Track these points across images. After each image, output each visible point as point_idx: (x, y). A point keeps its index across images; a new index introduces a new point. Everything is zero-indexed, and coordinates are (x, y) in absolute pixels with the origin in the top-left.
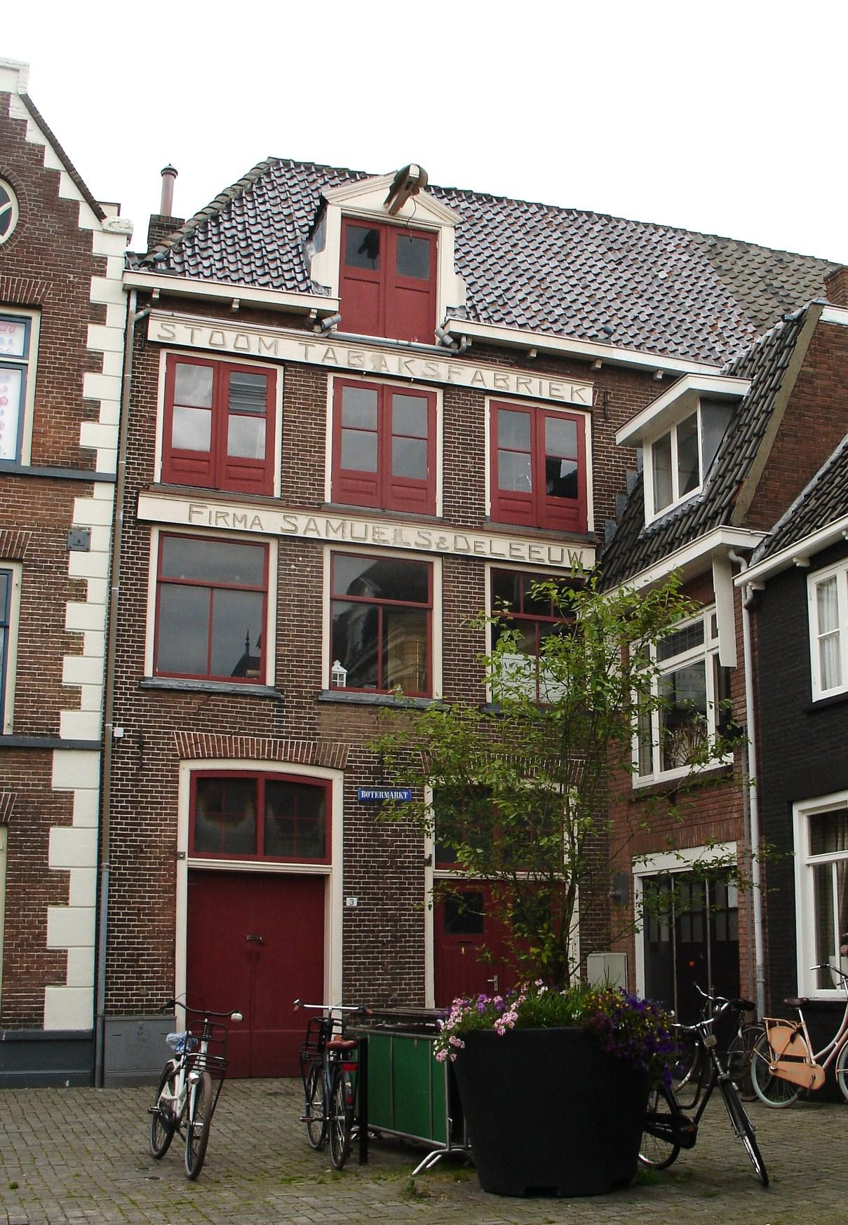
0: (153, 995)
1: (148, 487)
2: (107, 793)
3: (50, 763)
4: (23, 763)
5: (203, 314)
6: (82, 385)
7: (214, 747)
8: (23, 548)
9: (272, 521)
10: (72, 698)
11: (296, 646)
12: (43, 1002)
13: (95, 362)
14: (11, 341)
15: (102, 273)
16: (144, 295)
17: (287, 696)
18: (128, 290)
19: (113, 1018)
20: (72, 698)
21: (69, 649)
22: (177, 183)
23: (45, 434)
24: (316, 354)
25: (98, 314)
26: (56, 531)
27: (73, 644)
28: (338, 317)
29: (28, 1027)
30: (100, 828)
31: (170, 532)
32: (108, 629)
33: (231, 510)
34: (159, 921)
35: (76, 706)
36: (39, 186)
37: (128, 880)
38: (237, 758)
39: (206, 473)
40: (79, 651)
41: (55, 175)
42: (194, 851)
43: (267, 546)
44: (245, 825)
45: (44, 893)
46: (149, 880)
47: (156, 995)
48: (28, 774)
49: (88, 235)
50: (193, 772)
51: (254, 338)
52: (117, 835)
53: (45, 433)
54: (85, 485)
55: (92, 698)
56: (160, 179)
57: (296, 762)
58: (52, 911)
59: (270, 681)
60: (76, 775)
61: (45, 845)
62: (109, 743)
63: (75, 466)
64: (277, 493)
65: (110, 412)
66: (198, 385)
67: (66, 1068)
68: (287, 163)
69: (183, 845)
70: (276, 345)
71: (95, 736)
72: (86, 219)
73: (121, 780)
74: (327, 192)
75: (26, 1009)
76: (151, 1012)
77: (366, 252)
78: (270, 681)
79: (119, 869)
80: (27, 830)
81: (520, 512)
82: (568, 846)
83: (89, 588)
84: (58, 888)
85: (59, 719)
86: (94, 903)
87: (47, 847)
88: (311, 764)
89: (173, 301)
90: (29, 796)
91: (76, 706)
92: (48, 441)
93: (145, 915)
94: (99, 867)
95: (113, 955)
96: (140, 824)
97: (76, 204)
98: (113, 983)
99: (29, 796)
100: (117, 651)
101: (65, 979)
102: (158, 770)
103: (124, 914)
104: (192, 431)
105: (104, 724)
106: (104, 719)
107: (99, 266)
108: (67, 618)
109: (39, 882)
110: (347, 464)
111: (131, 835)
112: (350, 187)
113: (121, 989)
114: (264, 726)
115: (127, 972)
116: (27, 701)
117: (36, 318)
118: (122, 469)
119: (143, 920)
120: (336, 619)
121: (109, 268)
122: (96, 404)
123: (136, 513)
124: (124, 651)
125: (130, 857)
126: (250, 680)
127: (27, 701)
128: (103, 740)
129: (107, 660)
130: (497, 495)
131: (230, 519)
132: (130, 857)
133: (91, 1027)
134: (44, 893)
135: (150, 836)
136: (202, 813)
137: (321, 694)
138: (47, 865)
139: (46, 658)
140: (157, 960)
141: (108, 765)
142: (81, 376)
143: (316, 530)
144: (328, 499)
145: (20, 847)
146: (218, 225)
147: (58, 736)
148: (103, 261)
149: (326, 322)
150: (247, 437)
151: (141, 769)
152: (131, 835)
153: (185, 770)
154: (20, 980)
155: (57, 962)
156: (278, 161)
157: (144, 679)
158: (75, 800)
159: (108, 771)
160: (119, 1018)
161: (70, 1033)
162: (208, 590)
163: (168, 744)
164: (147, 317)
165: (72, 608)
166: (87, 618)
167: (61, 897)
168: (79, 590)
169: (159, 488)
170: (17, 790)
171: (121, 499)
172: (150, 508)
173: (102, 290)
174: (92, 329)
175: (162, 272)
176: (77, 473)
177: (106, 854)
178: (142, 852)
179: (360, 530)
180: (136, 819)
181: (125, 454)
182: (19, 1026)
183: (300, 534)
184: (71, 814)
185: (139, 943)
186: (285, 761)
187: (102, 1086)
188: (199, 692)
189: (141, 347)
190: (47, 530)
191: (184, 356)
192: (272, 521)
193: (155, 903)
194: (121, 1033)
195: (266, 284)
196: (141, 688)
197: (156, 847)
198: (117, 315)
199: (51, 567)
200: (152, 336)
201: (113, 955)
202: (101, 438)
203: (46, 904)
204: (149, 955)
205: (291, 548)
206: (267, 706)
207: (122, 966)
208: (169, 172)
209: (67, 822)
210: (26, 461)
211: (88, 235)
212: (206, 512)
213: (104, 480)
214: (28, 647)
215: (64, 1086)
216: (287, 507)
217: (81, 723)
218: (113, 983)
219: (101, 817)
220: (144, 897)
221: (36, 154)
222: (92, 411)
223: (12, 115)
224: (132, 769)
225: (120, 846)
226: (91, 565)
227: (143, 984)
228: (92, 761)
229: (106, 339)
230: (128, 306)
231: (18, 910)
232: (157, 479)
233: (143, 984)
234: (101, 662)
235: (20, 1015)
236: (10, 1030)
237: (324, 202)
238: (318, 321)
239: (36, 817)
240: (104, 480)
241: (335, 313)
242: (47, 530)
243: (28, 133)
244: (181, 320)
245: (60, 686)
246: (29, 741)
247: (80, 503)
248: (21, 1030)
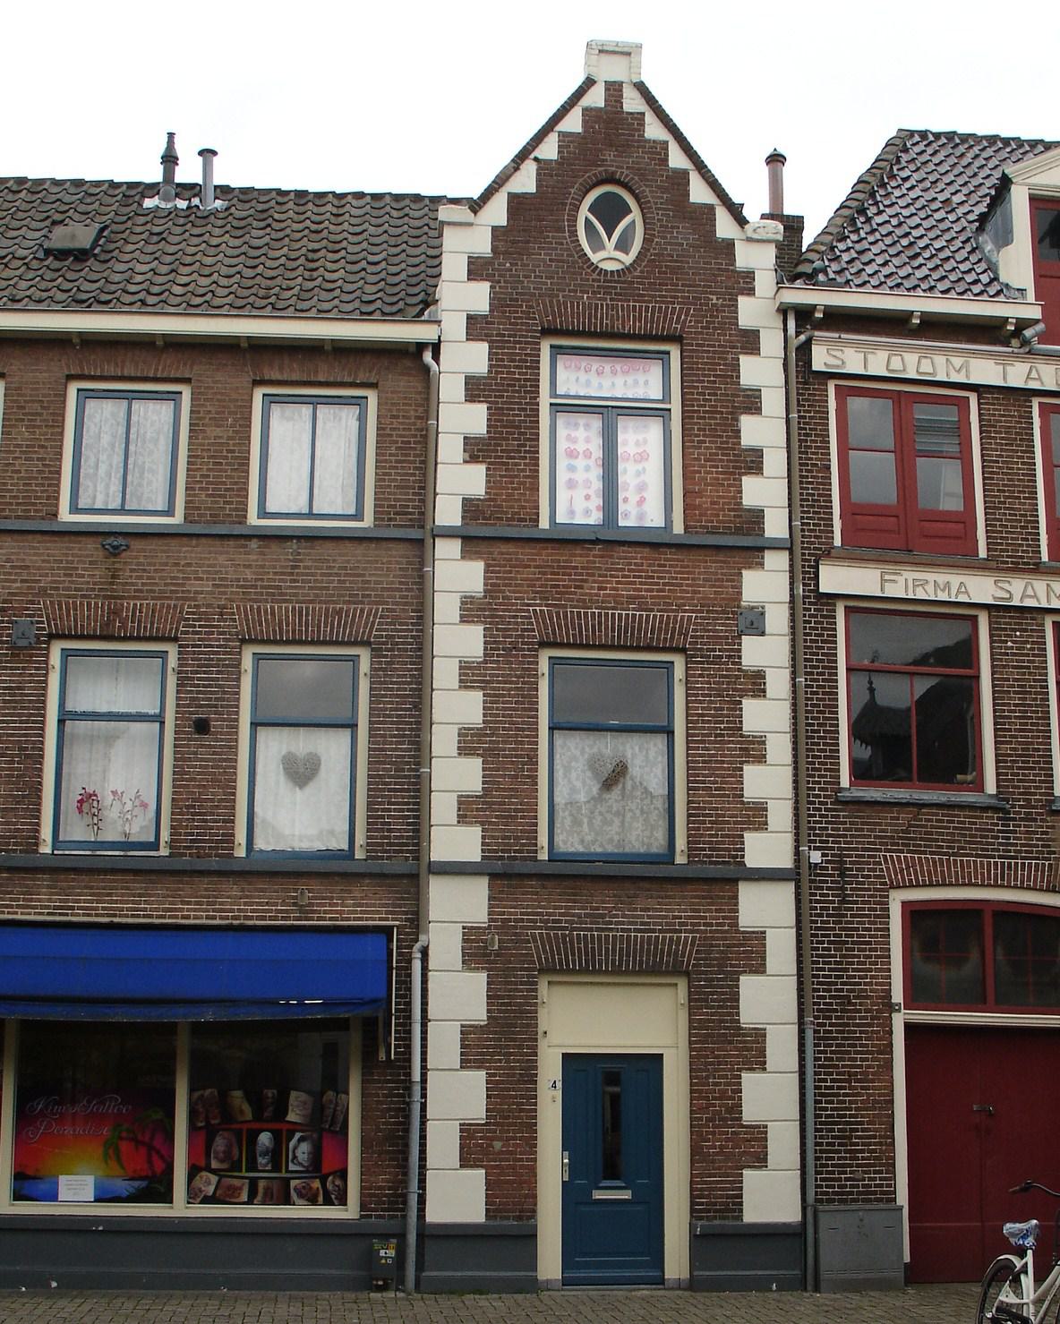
0: (870, 1179)
1: (828, 553)
2: (807, 933)
3: (736, 897)
4: (704, 897)
6: (739, 431)
7: (929, 872)
8: (686, 635)
9: (981, 589)
10: (756, 816)
11: (1020, 743)
12: (741, 1189)
14: (646, 383)
15: (750, 292)
16: (803, 315)
17: (1013, 806)
18: (784, 311)
19: (827, 1208)
20: (756, 816)
21: (749, 756)
22: (788, 171)
23: (700, 494)
24: (1017, 374)
25: (751, 342)
26: (724, 612)
27: (754, 750)
28: (1041, 327)
30: (800, 975)
31: (860, 607)
32: (795, 730)
33: (941, 577)
34: (874, 1088)
35: (762, 826)
37: (836, 1038)
38: (957, 885)
39: (898, 531)
40: (761, 759)
41: (684, 175)
42: (912, 1001)
43: (974, 619)
44: (969, 968)
45: (737, 1056)
46: (860, 1039)
47: (875, 1179)
48: (710, 911)
49: (729, 245)
50: (904, 904)
51: (940, 360)
52: (819, 983)
53: (700, 492)
54: (754, 553)
55: (781, 815)
56: (765, 170)
57: (1028, 888)
58: (748, 1079)
59: (991, 787)
60: (767, 911)
61: (735, 998)
62: (805, 870)
63: (739, 531)
64: (983, 553)
65: (776, 462)
66: (870, 416)
67: (771, 1269)
68: (923, 134)
69: (898, 996)
70: (965, 366)
71: (786, 862)
72: (724, 227)
73: (821, 915)
74: (1010, 170)
75: (722, 1196)
77: (1047, 241)
78: (991, 787)
79: (825, 1025)
80: (712, 980)
83: (768, 680)
84: (752, 1050)
85: (743, 843)
87: (737, 1000)
88: (1048, 890)
89: (841, 320)
91: (762, 826)
92: (704, 502)
93: (857, 1081)
94: (801, 1023)
95: (821, 1130)
96: (846, 970)
97: (711, 208)
98: (822, 1166)
100: (808, 757)
102: (863, 902)
103: (833, 1081)
104: (876, 477)
105: (797, 848)
108: (744, 719)
109: (730, 1042)
110: (858, 495)
111: (836, 984)
112: (1030, 161)
113: (833, 1172)
114: (988, 843)
115: (838, 1152)
116: (704, 822)
118: (798, 534)
119: (856, 1088)
121: (757, 284)
123: (817, 585)
124: (813, 757)
125: (836, 1010)
126: (963, 786)
127: (704, 822)
128: (798, 867)
129: (796, 768)
130: (849, 510)
131: (930, 588)
132: (836, 1010)
134: (737, 1056)
135: (860, 984)
136: (917, 955)
137: (1053, 802)
138: (738, 1021)
139: (724, 769)
141: (805, 898)
142: (737, 420)
143: (1035, 596)
144: (1045, 557)
145: (706, 1000)
148: (749, 276)
149: (1028, 333)
150: (942, 485)
151: (843, 902)
152: (836, 984)
153: (896, 900)
154: (713, 1162)
155: (755, 1140)
157: (841, 790)
158: (768, 942)
159: (805, 906)
160: (832, 1207)
161: (775, 1225)
163: (875, 870)
164: (809, 342)
165: (749, 706)
166: (767, 716)
168: (756, 684)
170: (698, 931)
172: (833, 578)
173: (753, 311)
175: (823, 284)
176: (740, 541)
177: (809, 1007)
178: (850, 1003)
180: (840, 963)
181: (798, 513)
182: (715, 1217)
183: (1015, 602)
184: (764, 959)
185: (851, 1116)
186: (1015, 887)
187: (817, 1289)
188: (908, 804)
189: (805, 379)
190: (713, 612)
191: (854, 386)
192: (981, 589)
193: (869, 1067)
194: (836, 1229)
195: (947, 291)
196: (838, 802)
197: (867, 997)
198: (772, 342)
199: (721, 657)
200: (817, 365)
201: (821, 1130)
202: (766, 493)
203: (740, 1070)
204: (863, 1130)
206: (989, 819)
207: (833, 1144)
208: (776, 160)
210: (678, 528)
211: (729, 245)
212: (901, 580)
213: (776, 546)
214: (700, 755)
216: (998, 569)
217: (768, 847)
218: (822, 1166)
219: (799, 962)
220: (855, 1060)
222: (753, 462)
224: (833, 902)
225: (824, 997)
226: (767, 652)
228: (786, 892)
229: (763, 372)
230: (785, 330)
231: (707, 1077)
232: (838, 542)
234: (789, 771)
235: (715, 1204)
237: (1005, 183)
240: (776, 546)
241: (1037, 321)
242: (713, 612)
244: (850, 343)
245: (743, 803)
246: (712, 871)
247: (748, 576)
248: (717, 1222)
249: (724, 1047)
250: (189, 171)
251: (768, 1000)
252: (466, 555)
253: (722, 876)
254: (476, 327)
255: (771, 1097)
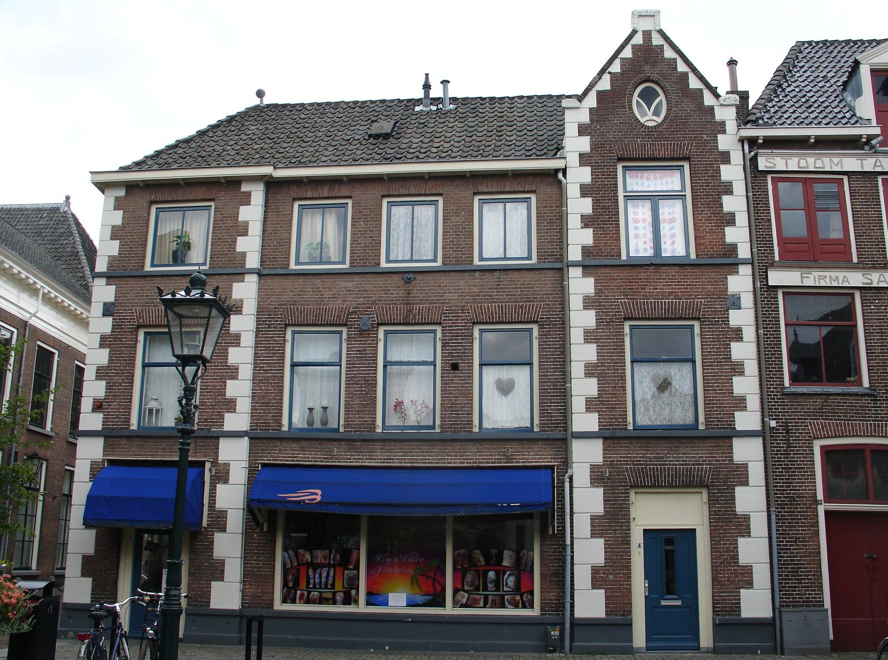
1: (772, 265)
5: (829, 149)
9: (856, 279)
10: (741, 403)
13: (728, 189)
14: (673, 182)
15: (724, 132)
16: (752, 142)
18: (742, 140)
20: (741, 403)
22: (738, 68)
24: (869, 164)
25: (725, 157)
27: (738, 369)
28: (881, 138)
29: (732, 615)
30: (767, 486)
31: (790, 292)
35: (744, 408)
36: (677, 83)
40: (742, 373)
41: (686, 75)
42: (827, 499)
43: (852, 295)
46: (800, 519)
49: (712, 108)
51: (826, 160)
54: (733, 267)
55: (753, 402)
58: (741, 540)
60: (748, 452)
61: (733, 499)
62: (767, 431)
63: (725, 256)
64: (855, 260)
65: (742, 219)
69: (820, 496)
70: (841, 162)
71: (757, 427)
74: (859, 57)
75: (729, 603)
76: (809, 606)
77: (881, 93)
81: (131, 277)
82: (389, 548)
84: (743, 526)
86: (767, 535)
89: (773, 143)
90: (720, 468)
91: (744, 408)
94: (769, 511)
96: (792, 483)
99: (720, 468)
101: (752, 584)
105: (763, 419)
106: (763, 415)
107: (721, 127)
112: (869, 51)
117: (687, 166)
118: (756, 256)
120: (790, 345)
122: (732, 215)
123: (767, 281)
126: (851, 384)
128: (764, 429)
131: (828, 280)
133: (771, 615)
136: (830, 474)
140: (810, 571)
141: (768, 445)
146: (783, 90)
147: (734, 428)
148: (723, 124)
149: (873, 142)
156: (803, 43)
157: (785, 388)
161: (759, 619)
162: (818, 328)
164: (756, 156)
166: (744, 351)
167: (746, 531)
169: (780, 264)
171: (757, 274)
172: (776, 278)
173: (725, 142)
174: (723, 167)
177: (772, 503)
178: (794, 500)
179: (814, 278)
184: (748, 478)
188: (821, 394)
191: (781, 176)
192: (856, 279)
194: (792, 621)
197: (804, 497)
198: (737, 157)
200: (761, 167)
202: (738, 235)
204: (805, 568)
205: (869, 295)
206: (867, 401)
208: (732, 63)
209: (746, 483)
210: (693, 256)
211: (712, 108)
212: (812, 276)
213: (744, 262)
215: (757, 654)
216: (864, 268)
217: (748, 419)
219: (766, 479)
221: (673, 63)
223: (654, 43)
226: (742, 318)
227: (803, 587)
228: (758, 443)
229: (733, 172)
230: (743, 150)
232: (777, 258)
233: (803, 587)
236: (720, 617)
237: (857, 64)
238: (868, 142)
239: (726, 480)
240: (744, 262)
241: (878, 136)
243: (665, 53)
246: (718, 432)
249: (728, 524)
250: (436, 92)
251: (750, 499)
252: (585, 275)
253: (723, 435)
254: (584, 159)
255: (753, 550)
